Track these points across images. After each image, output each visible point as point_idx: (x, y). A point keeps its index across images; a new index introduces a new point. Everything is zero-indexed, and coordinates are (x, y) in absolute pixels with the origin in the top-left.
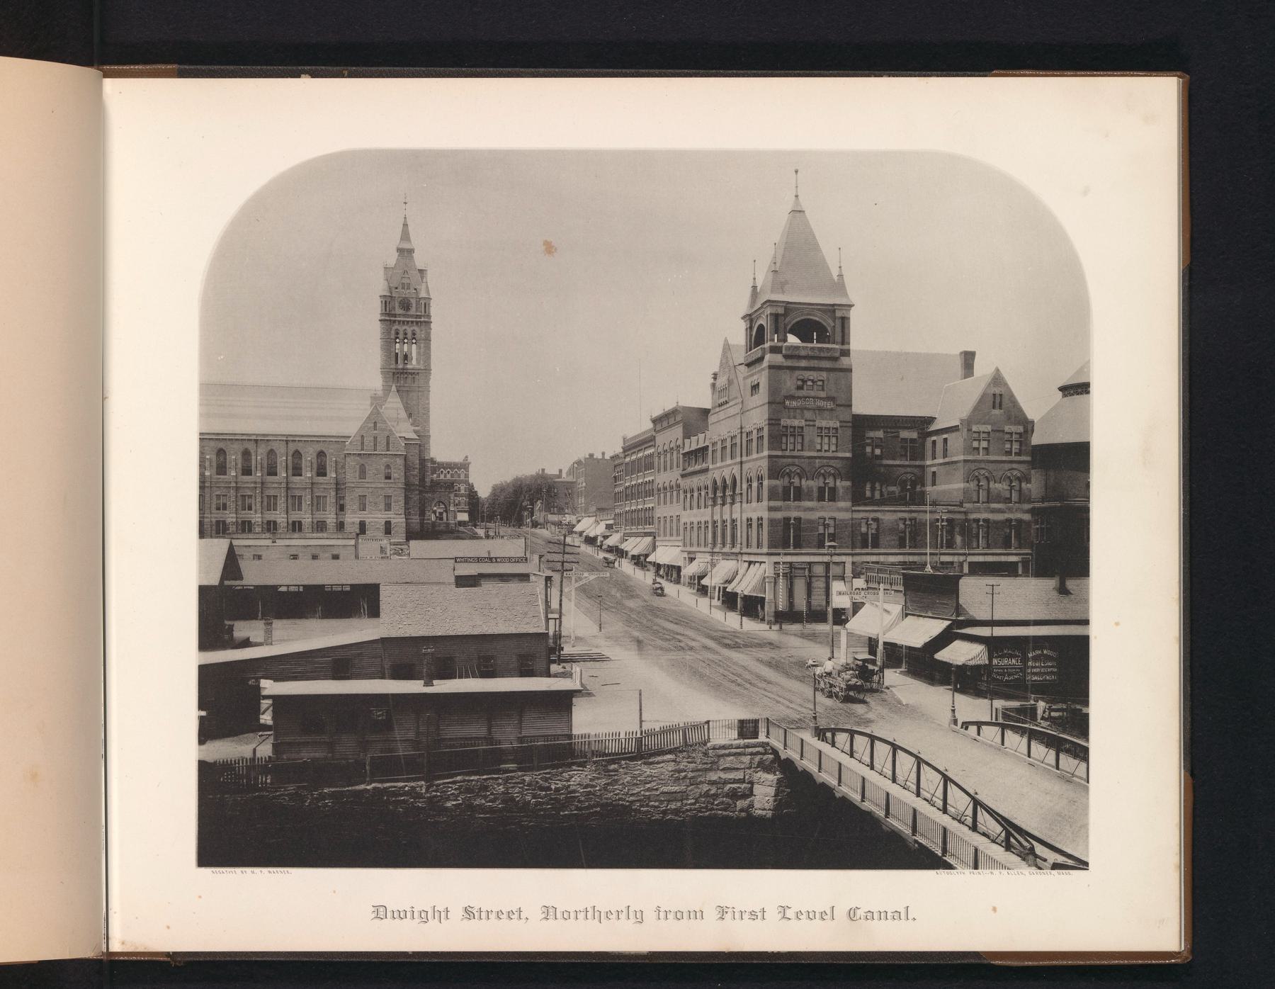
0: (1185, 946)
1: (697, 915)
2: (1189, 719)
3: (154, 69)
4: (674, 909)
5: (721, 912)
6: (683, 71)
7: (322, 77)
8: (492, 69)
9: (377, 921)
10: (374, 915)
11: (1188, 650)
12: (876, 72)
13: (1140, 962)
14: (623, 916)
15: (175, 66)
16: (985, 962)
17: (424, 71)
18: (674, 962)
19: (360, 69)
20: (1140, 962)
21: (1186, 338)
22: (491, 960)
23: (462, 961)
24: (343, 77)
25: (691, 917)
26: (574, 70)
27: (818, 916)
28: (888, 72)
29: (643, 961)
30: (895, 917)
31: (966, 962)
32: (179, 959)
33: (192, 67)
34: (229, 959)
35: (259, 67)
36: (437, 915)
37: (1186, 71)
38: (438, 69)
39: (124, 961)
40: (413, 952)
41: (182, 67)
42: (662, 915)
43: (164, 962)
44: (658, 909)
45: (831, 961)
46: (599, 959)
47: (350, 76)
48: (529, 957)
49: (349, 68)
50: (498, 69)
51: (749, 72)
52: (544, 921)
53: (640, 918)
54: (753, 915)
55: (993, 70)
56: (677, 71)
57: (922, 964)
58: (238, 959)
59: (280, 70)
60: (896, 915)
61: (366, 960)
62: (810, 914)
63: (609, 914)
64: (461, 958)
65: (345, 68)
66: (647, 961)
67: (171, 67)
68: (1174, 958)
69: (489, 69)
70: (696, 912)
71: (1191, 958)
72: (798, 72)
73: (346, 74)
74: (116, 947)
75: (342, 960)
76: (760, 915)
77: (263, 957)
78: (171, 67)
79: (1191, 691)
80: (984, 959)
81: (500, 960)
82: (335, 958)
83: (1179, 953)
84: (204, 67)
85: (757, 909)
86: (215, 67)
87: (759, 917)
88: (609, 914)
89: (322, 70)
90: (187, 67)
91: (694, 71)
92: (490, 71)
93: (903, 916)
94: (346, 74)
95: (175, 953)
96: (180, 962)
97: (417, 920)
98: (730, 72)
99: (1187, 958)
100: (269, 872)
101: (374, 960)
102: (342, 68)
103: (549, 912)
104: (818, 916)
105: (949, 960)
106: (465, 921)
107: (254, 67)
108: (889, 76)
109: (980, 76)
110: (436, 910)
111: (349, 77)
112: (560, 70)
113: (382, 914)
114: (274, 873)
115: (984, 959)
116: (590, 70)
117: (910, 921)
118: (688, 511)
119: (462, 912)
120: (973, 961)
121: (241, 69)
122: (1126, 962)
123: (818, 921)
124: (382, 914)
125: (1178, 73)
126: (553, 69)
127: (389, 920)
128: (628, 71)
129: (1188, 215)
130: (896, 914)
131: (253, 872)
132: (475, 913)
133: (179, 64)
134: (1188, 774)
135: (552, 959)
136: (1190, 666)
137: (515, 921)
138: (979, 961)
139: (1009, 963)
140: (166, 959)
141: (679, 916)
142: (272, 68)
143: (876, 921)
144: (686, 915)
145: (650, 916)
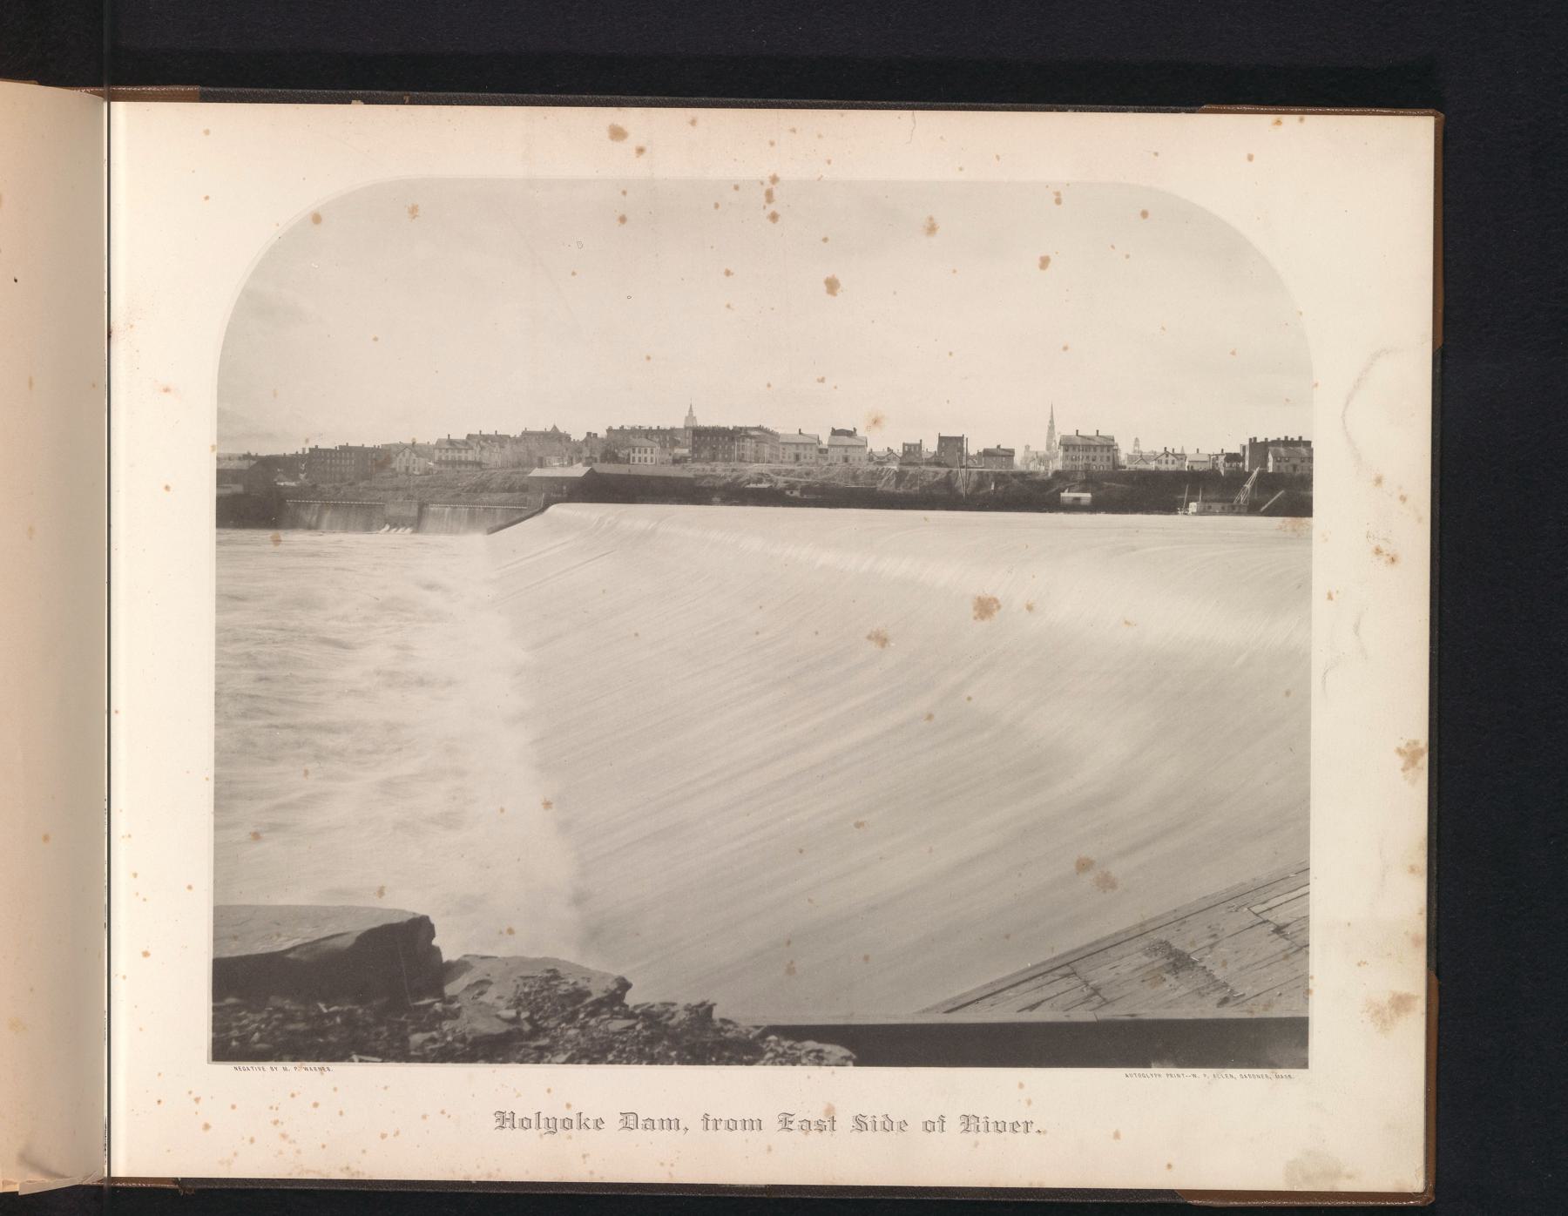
3: (172, 91)
5: (502, 1119)
7: (377, 103)
9: (626, 1131)
10: (621, 1125)
12: (1059, 106)
15: (197, 88)
16: (1181, 1201)
18: (797, 1196)
19: (424, 94)
22: (573, 1192)
23: (537, 1192)
25: (747, 1127)
26: (687, 99)
27: (1008, 1127)
29: (760, 1196)
32: (189, 1186)
33: (217, 90)
34: (250, 1187)
35: (300, 91)
38: (520, 95)
40: (478, 1182)
41: (205, 89)
42: (711, 1124)
43: (169, 1190)
44: (706, 1118)
45: (991, 1198)
47: (411, 103)
48: (620, 1189)
49: (411, 93)
50: (594, 96)
52: (964, 1134)
54: (928, 1127)
55: (1203, 105)
56: (814, 101)
58: (261, 1187)
60: (805, 1125)
61: (419, 1190)
62: (550, 1121)
64: (537, 1190)
65: (406, 93)
66: (765, 1195)
67: (192, 89)
71: (1434, 1199)
72: (963, 104)
73: (407, 101)
74: (121, 1169)
75: (390, 1190)
76: (828, 1125)
78: (192, 89)
81: (584, 1193)
84: (232, 90)
86: (246, 90)
89: (377, 94)
90: (212, 89)
93: (534, 1123)
94: (407, 101)
95: (184, 1180)
96: (190, 1190)
98: (880, 103)
99: (1429, 1199)
102: (402, 93)
103: (629, 1120)
104: (1008, 1127)
105: (1137, 1199)
106: (855, 1132)
108: (1075, 111)
109: (1041, 110)
113: (632, 1123)
116: (708, 99)
117: (682, 1131)
119: (851, 1123)
120: (1165, 1200)
122: (1354, 1203)
123: (814, 1134)
124: (632, 1123)
125: (1431, 111)
126: (662, 98)
127: (640, 1131)
128: (754, 101)
130: (649, 1123)
132: (867, 1121)
137: (1021, 1135)
139: (1210, 1203)
140: (173, 1186)
141: (731, 1125)
144: (739, 1125)
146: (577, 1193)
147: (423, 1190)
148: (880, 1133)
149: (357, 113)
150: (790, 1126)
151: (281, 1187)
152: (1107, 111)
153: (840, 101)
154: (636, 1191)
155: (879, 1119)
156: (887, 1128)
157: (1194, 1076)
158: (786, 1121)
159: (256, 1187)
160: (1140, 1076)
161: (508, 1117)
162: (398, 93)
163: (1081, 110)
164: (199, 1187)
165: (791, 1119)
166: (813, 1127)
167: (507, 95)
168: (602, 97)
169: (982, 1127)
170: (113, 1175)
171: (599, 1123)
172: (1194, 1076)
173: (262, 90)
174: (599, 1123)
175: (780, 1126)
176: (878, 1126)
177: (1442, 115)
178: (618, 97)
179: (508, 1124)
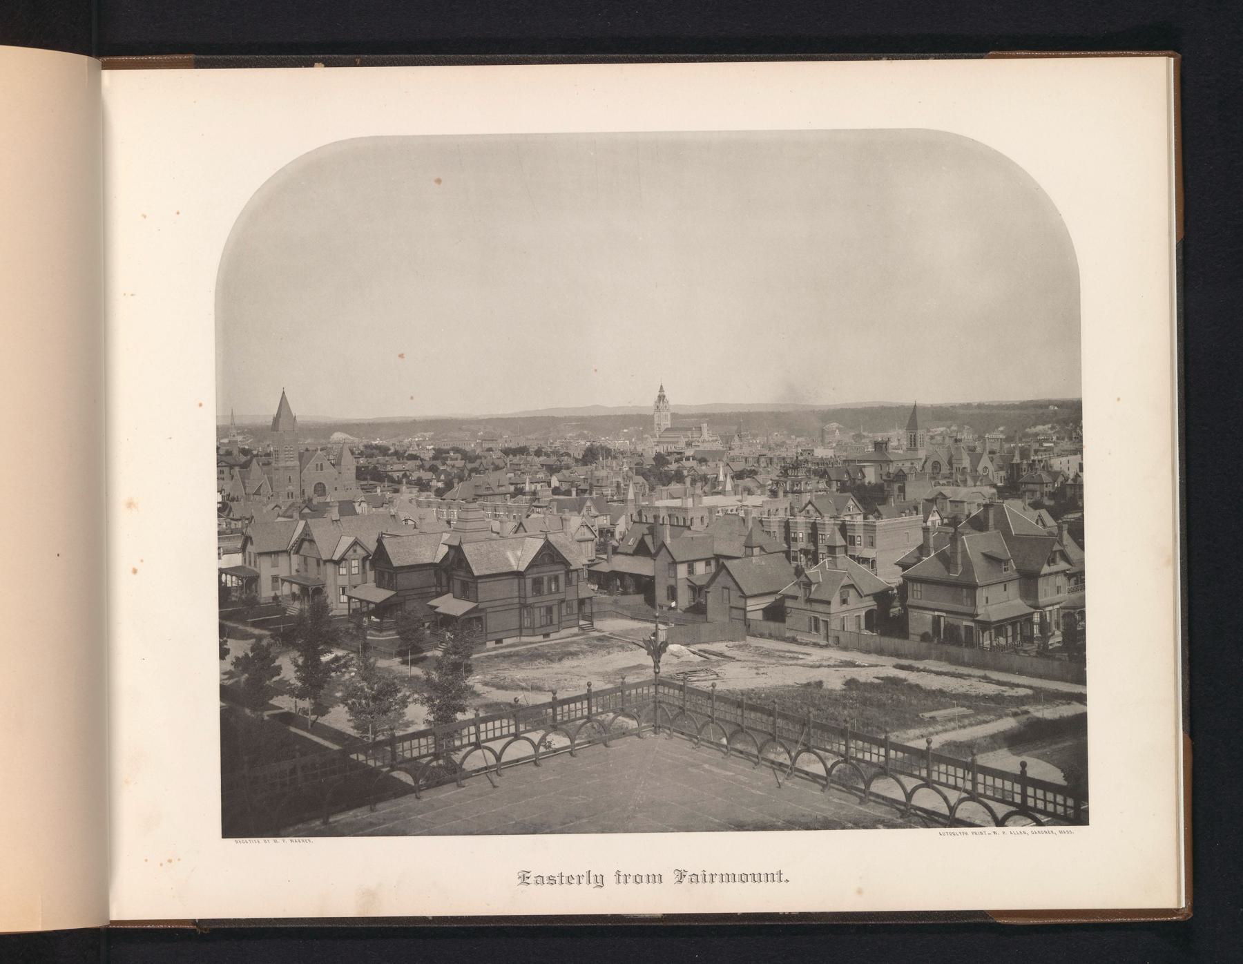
1: (656, 878)
2: (1188, 682)
4: (633, 874)
5: (522, 877)
6: (687, 55)
8: (500, 56)
11: (1186, 615)
13: (1142, 919)
14: (584, 881)
15: (192, 56)
16: (991, 921)
17: (434, 58)
20: (1142, 919)
21: (1180, 308)
22: (509, 925)
24: (355, 65)
25: (651, 881)
33: (208, 57)
35: (273, 56)
39: (151, 929)
40: (433, 917)
41: (198, 57)
42: (622, 879)
46: (615, 922)
47: (362, 64)
49: (361, 56)
53: (600, 882)
57: (930, 924)
59: (294, 59)
60: (540, 880)
62: (598, 878)
68: (1175, 915)
70: (773, 875)
71: (1192, 915)
73: (358, 63)
75: (364, 926)
76: (558, 880)
79: (1190, 655)
81: (518, 925)
83: (1178, 910)
84: (220, 57)
85: (700, 873)
87: (557, 882)
89: (335, 58)
93: (700, 878)
94: (358, 63)
96: (206, 930)
97: (593, 884)
99: (1188, 915)
100: (292, 841)
105: (957, 920)
114: (982, 833)
116: (596, 55)
118: (319, 471)
120: (979, 920)
122: (1129, 919)
125: (1170, 52)
128: (634, 56)
129: (1181, 191)
130: (694, 877)
131: (276, 842)
133: (196, 54)
134: (1187, 736)
135: (569, 923)
136: (1189, 630)
138: (985, 921)
141: (638, 879)
143: (700, 884)
144: (645, 879)
145: (610, 879)
147: (390, 926)
150: (528, 881)
151: (278, 926)
152: (914, 59)
153: (702, 55)
154: (559, 922)
156: (743, 880)
157: (995, 833)
158: (681, 875)
159: (257, 926)
160: (976, 834)
162: (351, 56)
163: (893, 58)
164: (213, 927)
165: (528, 875)
166: (545, 881)
167: (438, 56)
168: (513, 55)
172: (995, 833)
173: (243, 57)
175: (520, 881)
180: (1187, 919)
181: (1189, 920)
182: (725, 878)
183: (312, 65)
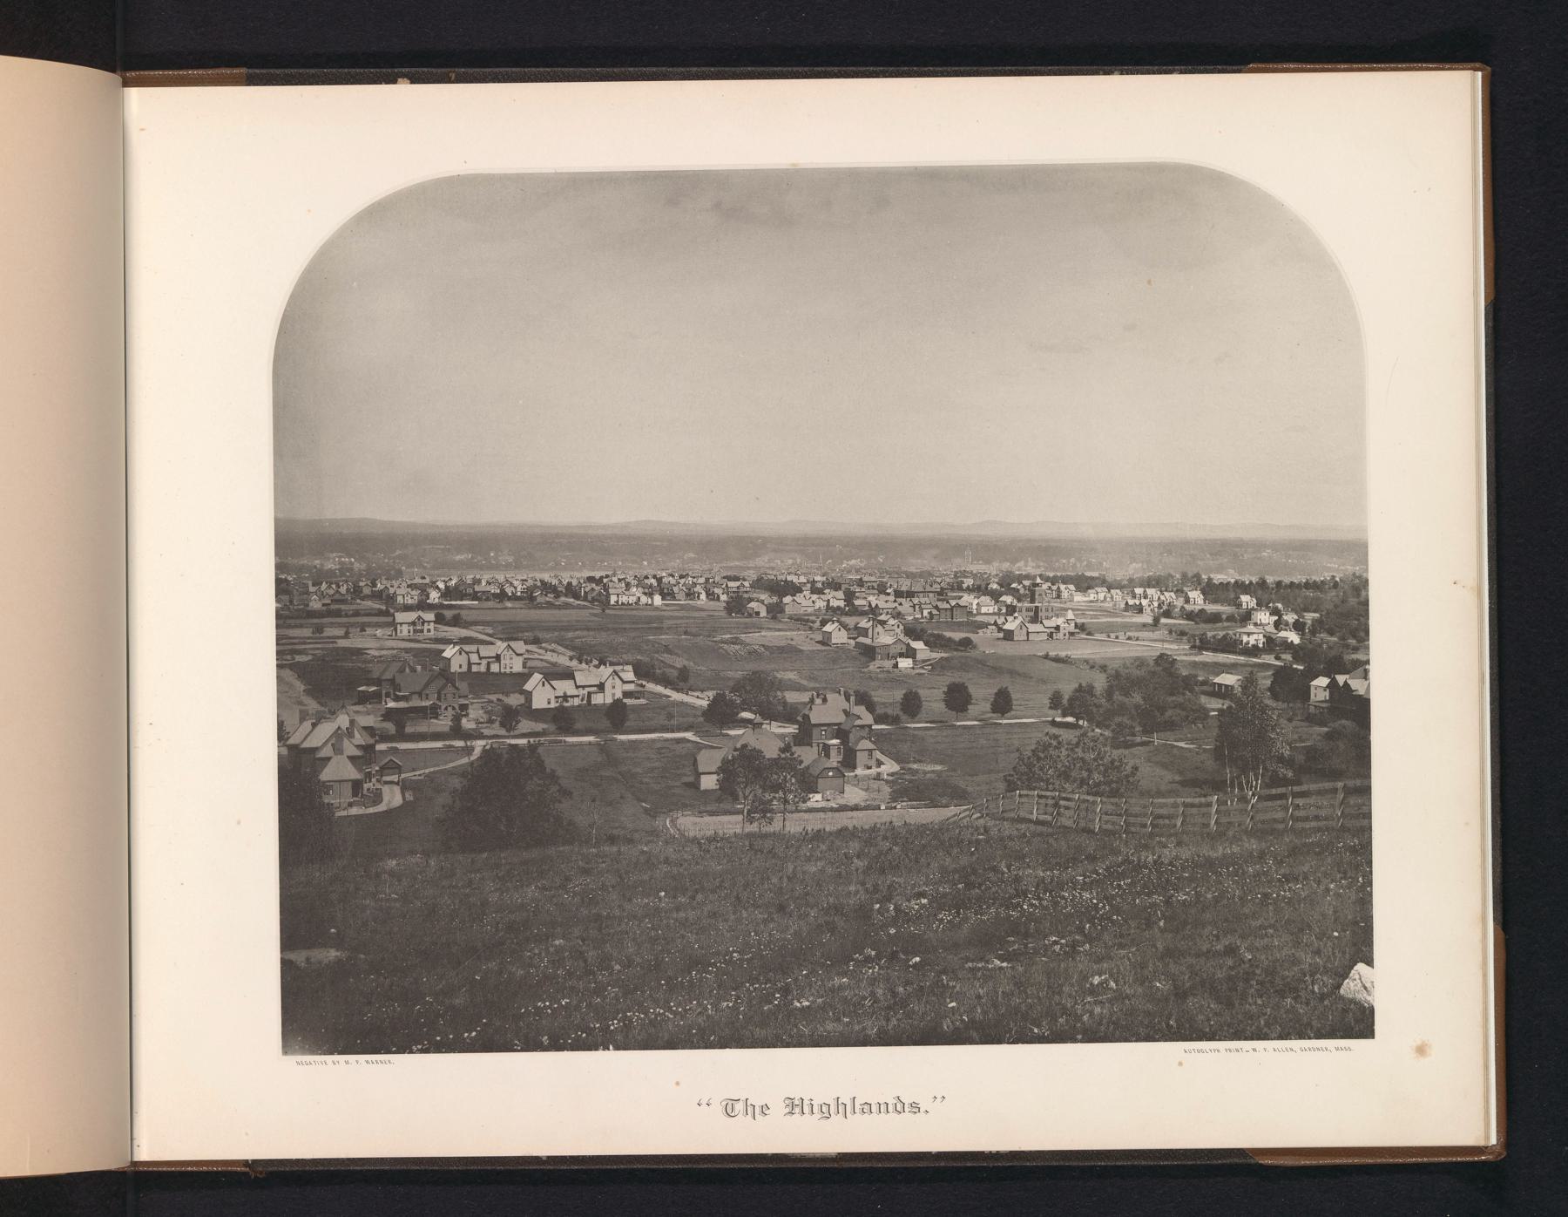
0: (1498, 1140)
3: (222, 74)
11: (1498, 775)
13: (1443, 1159)
15: (243, 70)
16: (1252, 1161)
20: (1443, 1159)
22: (644, 1166)
24: (450, 81)
28: (1120, 68)
30: (865, 1110)
31: (1228, 1161)
33: (264, 71)
35: (346, 70)
36: (841, 1108)
37: (1487, 63)
39: (192, 1172)
40: (548, 1157)
41: (251, 71)
48: (690, 1162)
51: (949, 69)
52: (788, 1117)
59: (372, 73)
60: (866, 1108)
63: (765, 1107)
69: (629, 69)
70: (887, 1104)
71: (1505, 1153)
73: (453, 78)
77: (363, 1165)
80: (1251, 1157)
82: (452, 1166)
84: (278, 71)
86: (292, 71)
88: (765, 1107)
90: (257, 71)
91: (881, 68)
92: (630, 72)
95: (255, 1162)
96: (261, 1173)
97: (817, 1115)
99: (1500, 1154)
101: (498, 1168)
102: (449, 70)
103: (794, 1106)
107: (340, 70)
110: (840, 1102)
111: (1367, 561)
112: (717, 69)
115: (1251, 1157)
121: (324, 73)
122: (1425, 1159)
125: (1477, 65)
142: (362, 71)
146: (648, 1167)
148: (893, 1115)
149: (404, 93)
153: (886, 69)
155: (891, 1102)
157: (1254, 1050)
161: (797, 1103)
166: (906, 1109)
169: (806, 1109)
170: (136, 1159)
171: (764, 1109)
172: (1254, 1050)
174: (764, 1109)
176: (891, 1108)
177: (1489, 69)
178: (664, 69)
179: (797, 1110)
180: (1499, 1158)
181: (1500, 1161)
182: (883, 1108)
183: (394, 82)
